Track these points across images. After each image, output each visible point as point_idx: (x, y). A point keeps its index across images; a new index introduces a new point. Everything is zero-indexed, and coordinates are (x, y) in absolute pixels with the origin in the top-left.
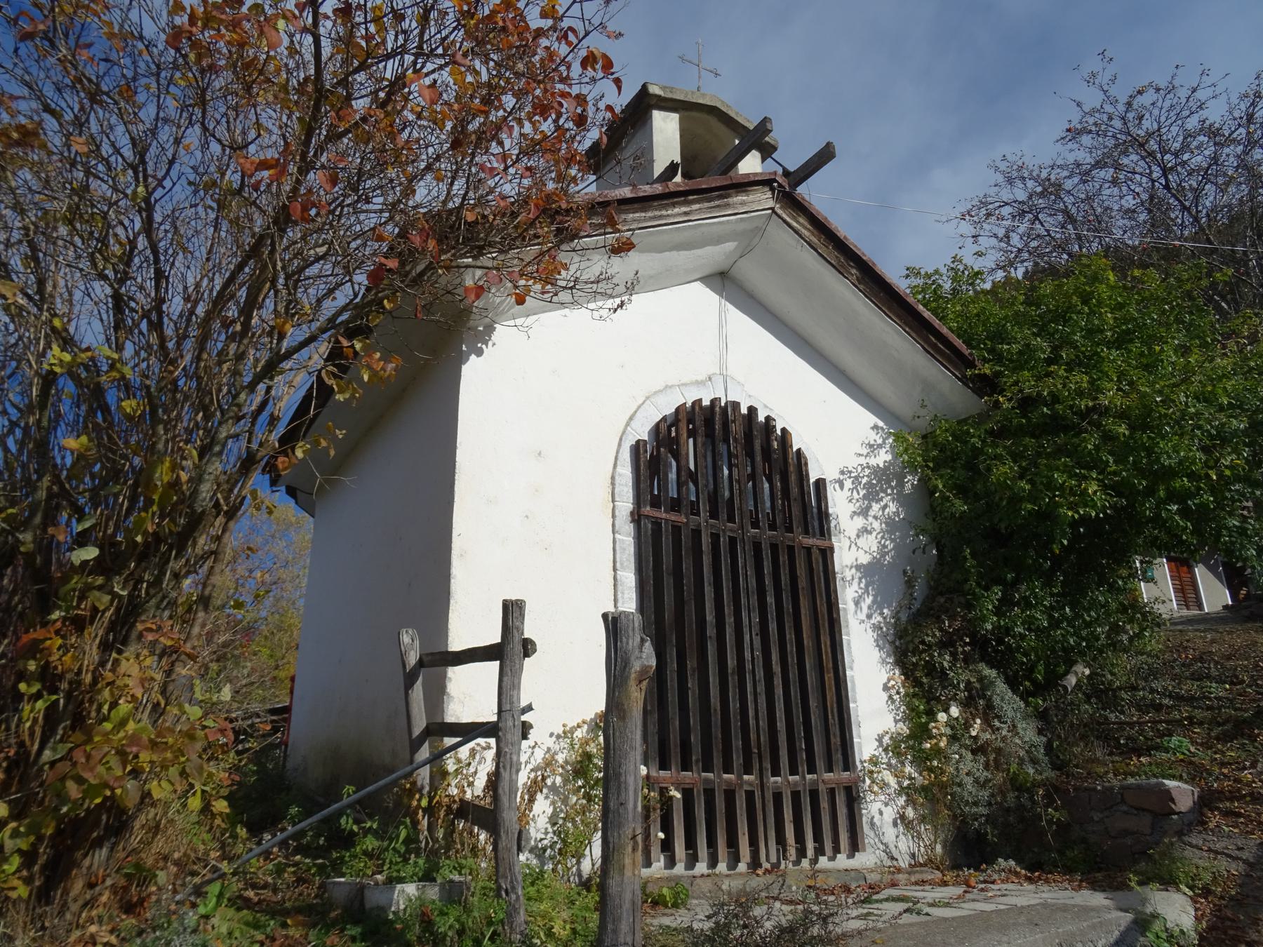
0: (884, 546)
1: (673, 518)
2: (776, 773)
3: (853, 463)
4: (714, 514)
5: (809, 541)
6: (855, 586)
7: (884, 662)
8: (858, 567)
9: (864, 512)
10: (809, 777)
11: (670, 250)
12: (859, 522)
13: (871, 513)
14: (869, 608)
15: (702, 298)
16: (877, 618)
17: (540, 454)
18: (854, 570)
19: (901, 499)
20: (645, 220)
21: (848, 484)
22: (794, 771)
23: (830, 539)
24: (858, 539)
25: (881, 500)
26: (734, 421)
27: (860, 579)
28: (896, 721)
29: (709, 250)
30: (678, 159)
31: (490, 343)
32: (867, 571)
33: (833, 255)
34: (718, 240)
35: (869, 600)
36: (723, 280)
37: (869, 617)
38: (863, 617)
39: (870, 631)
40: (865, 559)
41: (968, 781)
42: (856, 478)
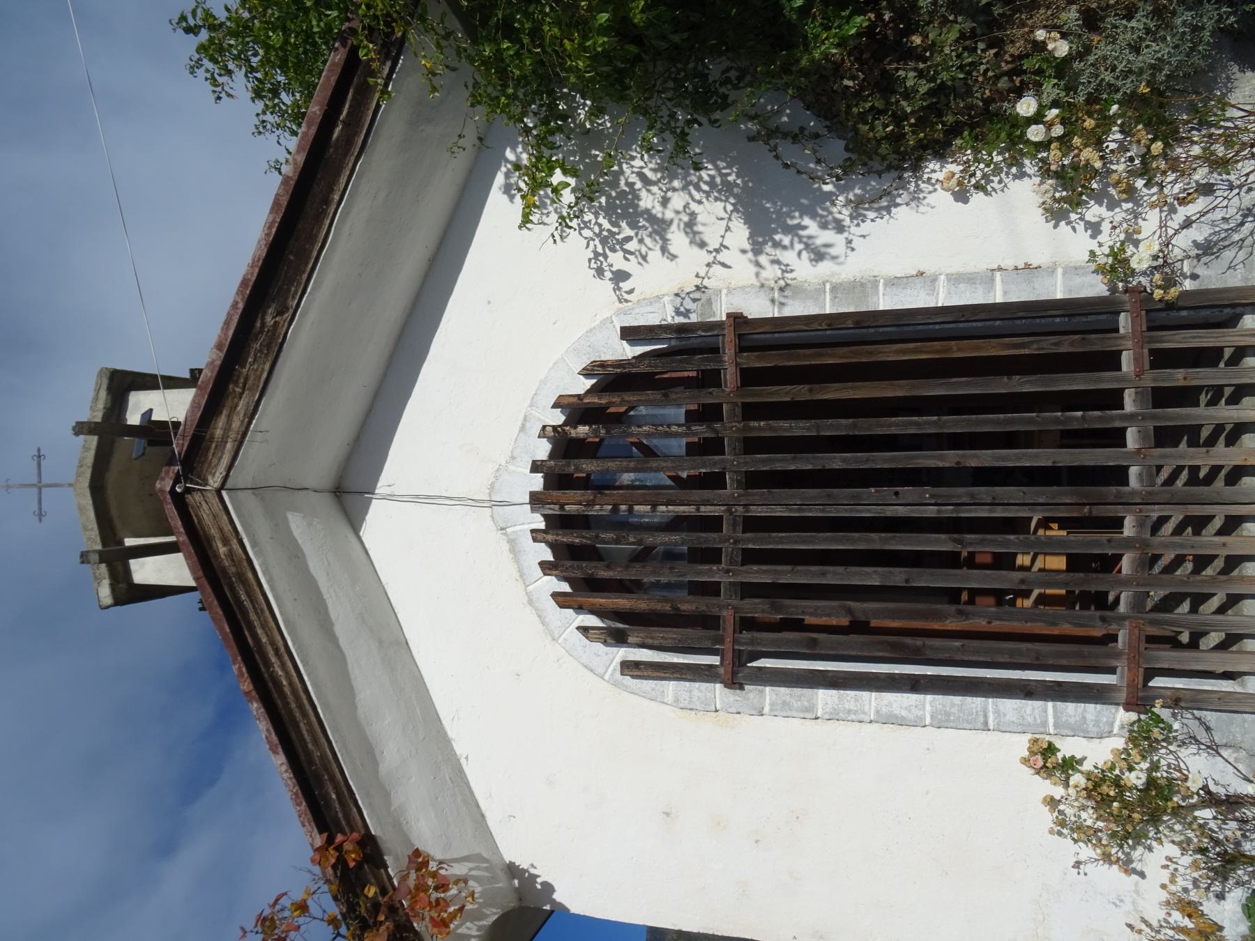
0: (712, 183)
1: (730, 630)
2: (1118, 475)
3: (577, 246)
4: (711, 556)
5: (730, 376)
6: (788, 257)
7: (916, 198)
8: (757, 251)
9: (660, 227)
10: (1129, 405)
11: (333, 639)
12: (678, 239)
13: (658, 210)
14: (824, 226)
15: (382, 525)
16: (842, 212)
17: (667, 814)
18: (763, 259)
19: (620, 146)
20: (309, 724)
21: (616, 260)
22: (1116, 438)
23: (719, 325)
24: (710, 259)
25: (631, 185)
26: (562, 508)
27: (777, 245)
28: (1021, 175)
29: (316, 566)
30: (182, 419)
31: (532, 871)
32: (763, 231)
33: (251, 368)
34: (296, 556)
35: (812, 227)
36: (349, 493)
37: (840, 228)
38: (838, 240)
39: (866, 227)
40: (740, 234)
41: (1153, 51)
42: (604, 242)
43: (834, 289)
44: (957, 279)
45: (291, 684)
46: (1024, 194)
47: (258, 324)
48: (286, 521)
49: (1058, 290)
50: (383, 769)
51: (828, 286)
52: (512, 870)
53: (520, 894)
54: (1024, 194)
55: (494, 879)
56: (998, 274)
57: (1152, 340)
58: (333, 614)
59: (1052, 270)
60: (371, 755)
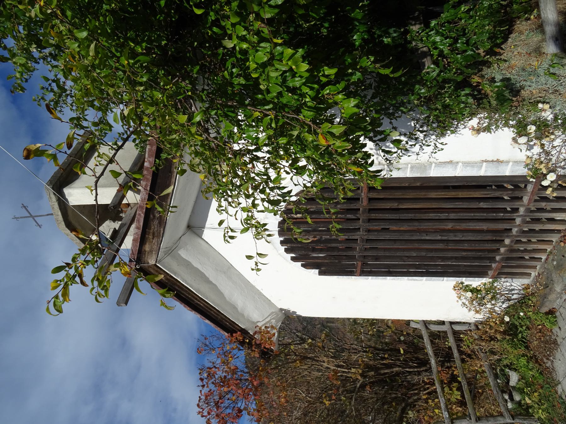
34: (188, 265)
43: (412, 168)
44: (467, 164)
45: (204, 304)
46: (507, 133)
47: (152, 216)
48: (179, 255)
49: (507, 171)
50: (239, 309)
51: (409, 165)
52: (281, 310)
53: (285, 314)
54: (507, 133)
55: (278, 315)
56: (485, 164)
57: (539, 194)
58: (207, 275)
59: (508, 162)
60: (234, 308)
